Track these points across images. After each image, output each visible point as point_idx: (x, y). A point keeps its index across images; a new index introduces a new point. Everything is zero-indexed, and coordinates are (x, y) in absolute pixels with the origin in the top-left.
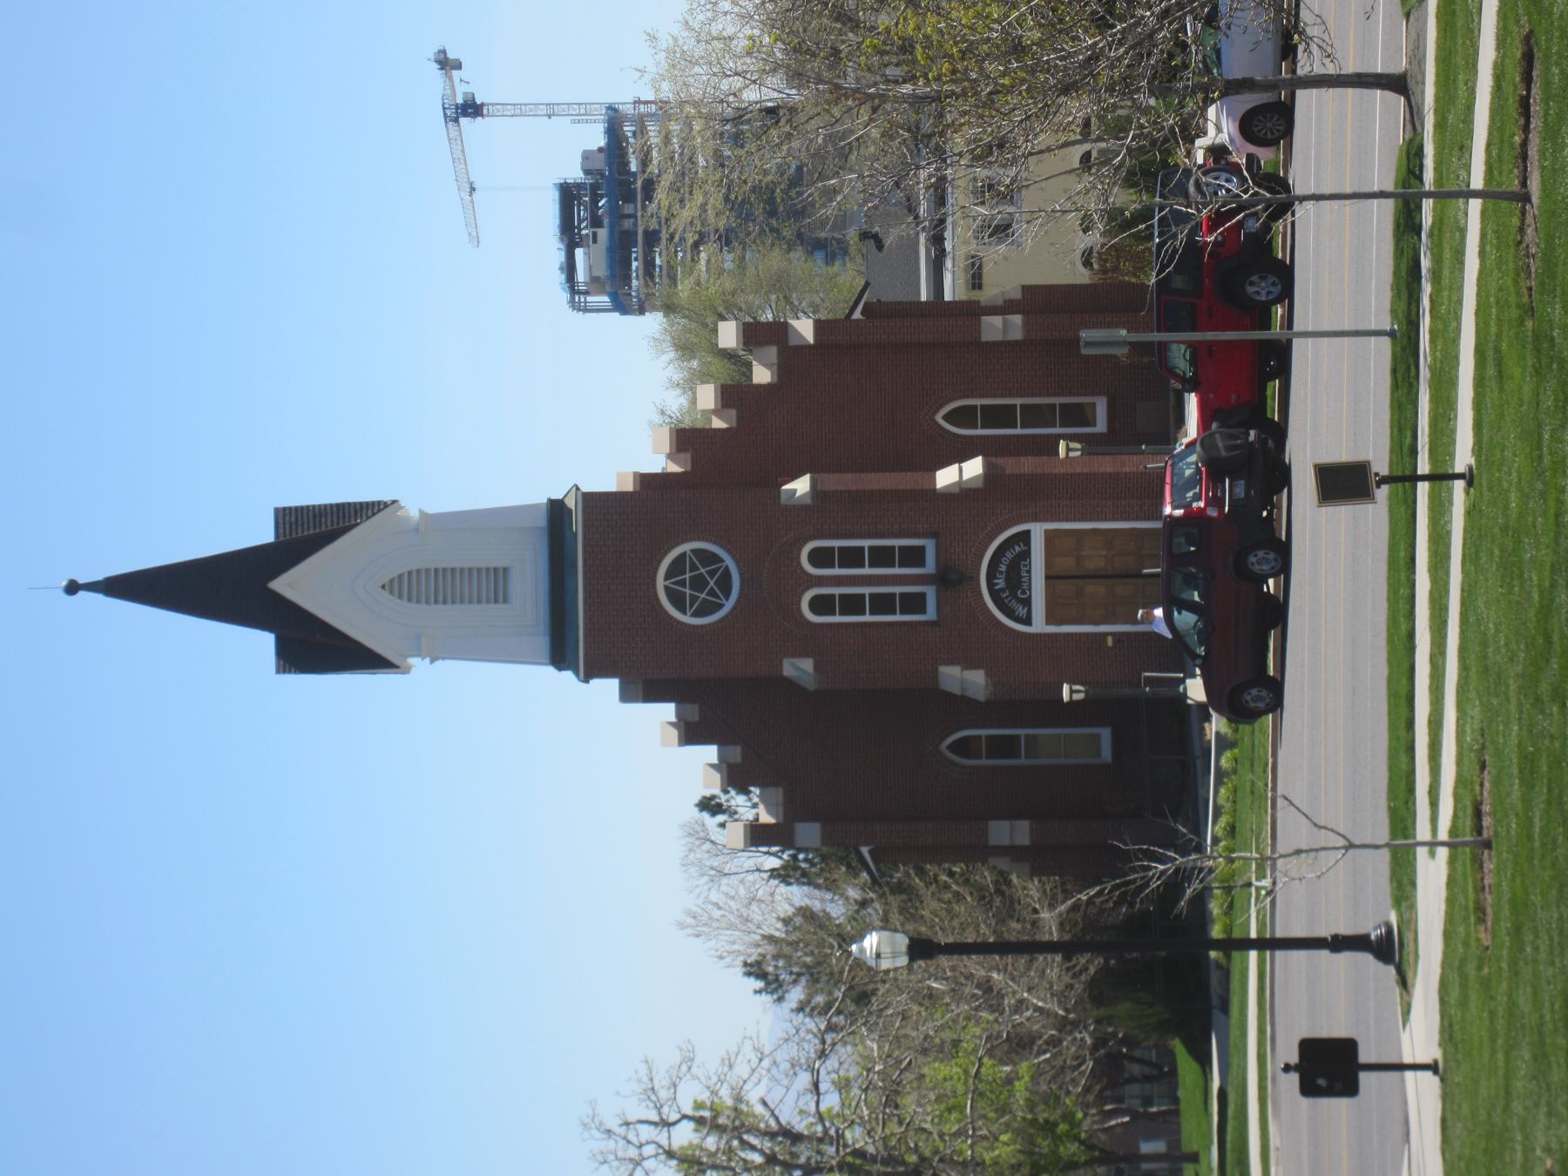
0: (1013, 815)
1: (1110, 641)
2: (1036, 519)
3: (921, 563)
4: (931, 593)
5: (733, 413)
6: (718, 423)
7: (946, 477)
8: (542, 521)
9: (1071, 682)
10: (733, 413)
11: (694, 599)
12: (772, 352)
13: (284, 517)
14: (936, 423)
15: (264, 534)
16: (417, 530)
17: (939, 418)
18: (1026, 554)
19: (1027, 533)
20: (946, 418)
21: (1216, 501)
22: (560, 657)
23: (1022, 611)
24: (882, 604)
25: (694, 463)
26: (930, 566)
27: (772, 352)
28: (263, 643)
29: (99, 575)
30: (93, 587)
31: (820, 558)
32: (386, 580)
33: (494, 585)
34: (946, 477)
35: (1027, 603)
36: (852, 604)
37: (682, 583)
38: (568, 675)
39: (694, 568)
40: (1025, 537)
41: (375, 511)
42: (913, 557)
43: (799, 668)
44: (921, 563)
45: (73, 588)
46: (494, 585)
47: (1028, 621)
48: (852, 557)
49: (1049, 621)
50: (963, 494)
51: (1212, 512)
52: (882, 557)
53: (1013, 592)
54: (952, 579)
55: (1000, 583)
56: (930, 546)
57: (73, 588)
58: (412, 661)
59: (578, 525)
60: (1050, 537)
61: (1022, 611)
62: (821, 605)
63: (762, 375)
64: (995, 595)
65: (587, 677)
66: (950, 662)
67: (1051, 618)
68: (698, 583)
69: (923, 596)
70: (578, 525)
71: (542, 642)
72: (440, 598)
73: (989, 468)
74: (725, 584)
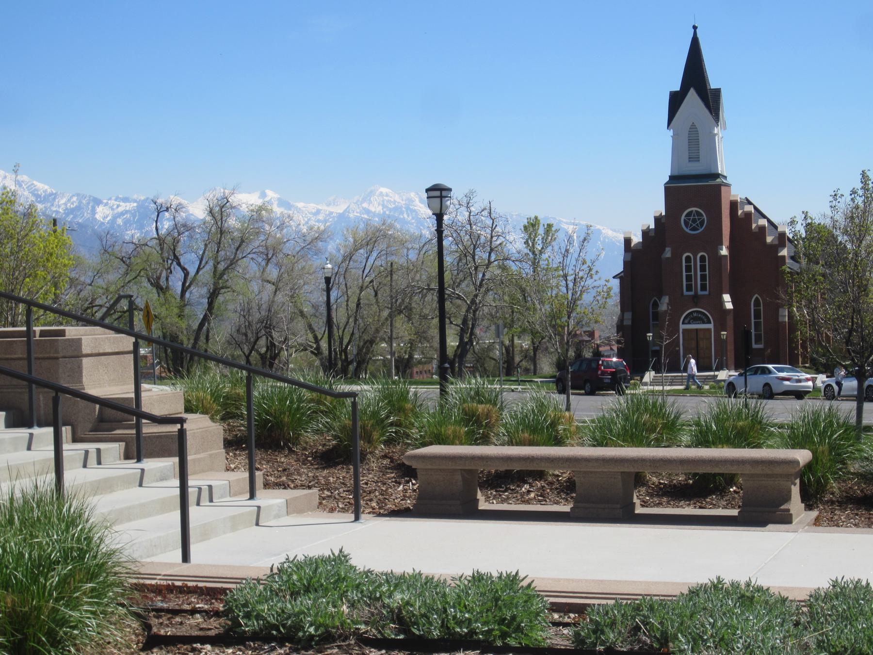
0: (633, 320)
1: (677, 349)
2: (715, 326)
3: (702, 290)
4: (692, 293)
5: (757, 230)
6: (754, 226)
7: (727, 297)
8: (713, 171)
9: (653, 336)
10: (757, 230)
11: (689, 219)
12: (776, 242)
13: (717, 92)
14: (687, 296)
15: (713, 84)
16: (711, 133)
17: (756, 295)
18: (704, 323)
19: (710, 323)
20: (757, 297)
21: (603, 373)
22: (672, 178)
23: (686, 321)
24: (689, 278)
25: (742, 219)
26: (700, 293)
27: (776, 242)
28: (677, 87)
29: (699, 35)
30: (695, 33)
31: (703, 259)
32: (695, 124)
33: (694, 157)
34: (727, 297)
35: (689, 323)
36: (688, 269)
37: (694, 216)
38: (668, 179)
39: (699, 219)
40: (709, 322)
41: (107, 321)
42: (703, 288)
43: (668, 253)
44: (702, 290)
45: (695, 28)
46: (694, 157)
47: (683, 323)
48: (703, 268)
49: (683, 330)
50: (721, 302)
51: (599, 372)
52: (703, 278)
53: (691, 319)
54: (696, 300)
55: (695, 315)
56: (706, 293)
57: (695, 28)
58: (672, 130)
59: (711, 183)
60: (709, 330)
61: (686, 321)
62: (688, 259)
63: (769, 239)
64: (691, 313)
65: (666, 188)
66: (670, 299)
67: (684, 331)
68: (694, 221)
69: (692, 291)
70: (711, 183)
71: (676, 173)
72: (690, 141)
73: (730, 310)
74: (694, 229)
